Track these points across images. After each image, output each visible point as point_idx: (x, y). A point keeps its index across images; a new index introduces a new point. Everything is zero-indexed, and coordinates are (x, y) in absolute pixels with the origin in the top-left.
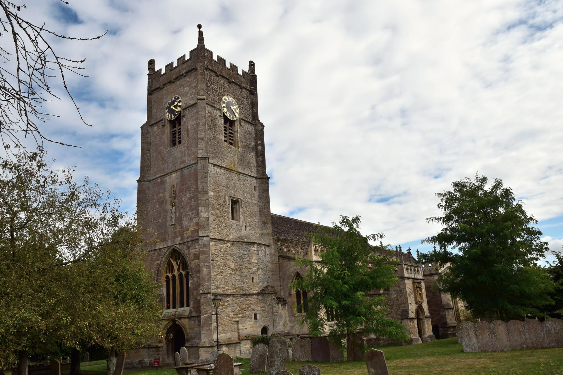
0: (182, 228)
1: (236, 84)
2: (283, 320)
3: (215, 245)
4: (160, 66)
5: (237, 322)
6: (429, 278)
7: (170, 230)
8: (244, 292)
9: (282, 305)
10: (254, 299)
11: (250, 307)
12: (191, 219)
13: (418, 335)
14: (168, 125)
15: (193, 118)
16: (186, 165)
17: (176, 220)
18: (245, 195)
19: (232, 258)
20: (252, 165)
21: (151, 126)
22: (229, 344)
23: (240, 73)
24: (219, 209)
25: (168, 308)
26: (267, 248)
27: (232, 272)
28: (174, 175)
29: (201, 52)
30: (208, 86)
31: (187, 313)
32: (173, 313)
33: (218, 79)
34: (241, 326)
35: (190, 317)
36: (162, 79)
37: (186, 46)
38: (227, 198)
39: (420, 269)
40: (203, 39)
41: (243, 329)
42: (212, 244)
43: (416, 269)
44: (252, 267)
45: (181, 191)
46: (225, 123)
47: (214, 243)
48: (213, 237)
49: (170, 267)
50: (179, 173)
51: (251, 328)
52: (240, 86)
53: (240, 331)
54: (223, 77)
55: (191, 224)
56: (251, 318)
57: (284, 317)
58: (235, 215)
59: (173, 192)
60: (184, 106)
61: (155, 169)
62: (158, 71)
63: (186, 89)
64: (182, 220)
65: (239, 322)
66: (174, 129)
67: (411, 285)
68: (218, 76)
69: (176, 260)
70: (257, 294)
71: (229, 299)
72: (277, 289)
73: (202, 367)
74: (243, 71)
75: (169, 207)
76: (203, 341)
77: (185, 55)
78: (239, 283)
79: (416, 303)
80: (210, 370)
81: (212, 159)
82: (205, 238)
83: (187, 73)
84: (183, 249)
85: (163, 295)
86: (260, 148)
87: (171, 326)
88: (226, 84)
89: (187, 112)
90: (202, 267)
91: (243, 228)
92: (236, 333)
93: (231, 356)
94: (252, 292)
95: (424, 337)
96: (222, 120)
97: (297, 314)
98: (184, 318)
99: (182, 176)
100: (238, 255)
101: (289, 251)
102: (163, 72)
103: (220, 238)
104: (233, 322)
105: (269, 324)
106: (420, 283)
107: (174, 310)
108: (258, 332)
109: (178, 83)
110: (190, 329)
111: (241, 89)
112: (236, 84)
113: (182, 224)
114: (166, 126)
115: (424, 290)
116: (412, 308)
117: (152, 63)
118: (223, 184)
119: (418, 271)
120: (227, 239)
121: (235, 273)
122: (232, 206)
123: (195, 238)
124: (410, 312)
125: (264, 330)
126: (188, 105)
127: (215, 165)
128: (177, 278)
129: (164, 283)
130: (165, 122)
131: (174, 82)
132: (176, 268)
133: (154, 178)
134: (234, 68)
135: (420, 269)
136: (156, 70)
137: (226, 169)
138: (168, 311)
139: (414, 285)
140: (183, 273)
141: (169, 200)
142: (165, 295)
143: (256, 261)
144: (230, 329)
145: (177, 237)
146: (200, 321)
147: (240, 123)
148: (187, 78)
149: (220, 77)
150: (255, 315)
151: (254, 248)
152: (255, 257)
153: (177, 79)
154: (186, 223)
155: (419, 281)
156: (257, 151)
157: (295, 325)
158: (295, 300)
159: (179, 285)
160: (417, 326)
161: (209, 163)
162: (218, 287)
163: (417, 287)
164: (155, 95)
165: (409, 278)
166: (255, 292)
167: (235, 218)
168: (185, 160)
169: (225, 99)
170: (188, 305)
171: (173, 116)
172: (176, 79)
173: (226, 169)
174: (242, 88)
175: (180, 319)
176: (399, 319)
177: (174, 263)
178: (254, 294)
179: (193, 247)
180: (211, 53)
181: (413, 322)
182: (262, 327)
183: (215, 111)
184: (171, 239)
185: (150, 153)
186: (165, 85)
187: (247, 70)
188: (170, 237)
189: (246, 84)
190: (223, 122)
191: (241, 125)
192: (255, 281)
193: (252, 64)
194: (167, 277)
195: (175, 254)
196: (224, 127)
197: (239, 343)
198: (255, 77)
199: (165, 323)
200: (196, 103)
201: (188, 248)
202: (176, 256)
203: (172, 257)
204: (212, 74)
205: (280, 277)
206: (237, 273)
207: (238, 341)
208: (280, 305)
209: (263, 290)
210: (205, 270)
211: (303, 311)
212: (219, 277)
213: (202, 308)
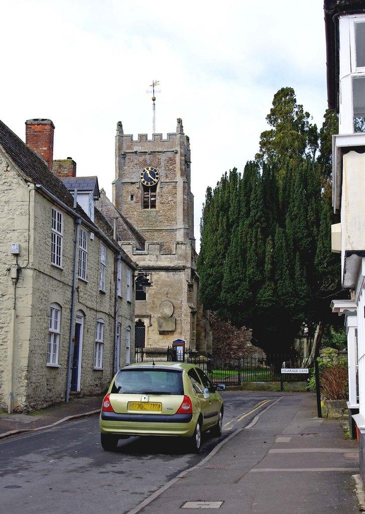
37: (167, 128)
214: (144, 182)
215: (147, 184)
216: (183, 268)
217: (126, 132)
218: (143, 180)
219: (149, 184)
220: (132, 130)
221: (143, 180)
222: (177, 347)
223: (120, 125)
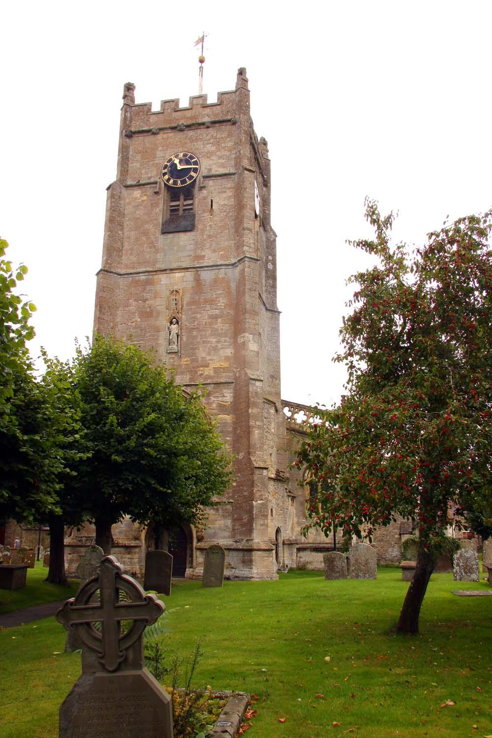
14: (164, 194)
37: (217, 84)
50: (189, 275)
63: (210, 148)
76: (256, 540)
90: (253, 427)
99: (198, 280)
109: (191, 133)
126: (213, 172)
131: (182, 130)
133: (132, 271)
154: (204, 355)
156: (267, 270)
164: (138, 140)
168: (204, 256)
171: (171, 181)
172: (188, 126)
185: (122, 229)
213: (255, 490)
214: (168, 180)
215: (175, 183)
216: (233, 383)
217: (140, 98)
218: (167, 177)
219: (179, 184)
220: (151, 95)
221: (167, 177)
222: (28, 569)
223: (129, 88)
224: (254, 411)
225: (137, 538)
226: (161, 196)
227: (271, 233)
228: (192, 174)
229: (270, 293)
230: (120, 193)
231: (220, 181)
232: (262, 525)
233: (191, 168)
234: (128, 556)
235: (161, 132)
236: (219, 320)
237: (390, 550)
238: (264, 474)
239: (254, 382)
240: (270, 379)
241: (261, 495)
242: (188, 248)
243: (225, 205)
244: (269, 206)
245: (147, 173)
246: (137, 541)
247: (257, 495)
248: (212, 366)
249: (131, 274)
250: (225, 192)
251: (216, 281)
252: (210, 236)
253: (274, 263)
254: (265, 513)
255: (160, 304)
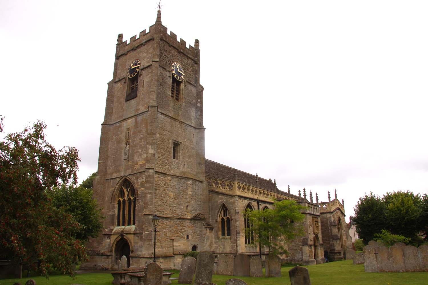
0: (133, 162)
1: (184, 54)
2: (210, 241)
3: (158, 177)
4: (126, 38)
5: (173, 240)
6: (323, 215)
7: (124, 163)
8: (180, 217)
9: (209, 229)
10: (187, 223)
11: (184, 229)
12: (141, 155)
13: (314, 257)
15: (148, 76)
16: (140, 113)
17: (129, 155)
18: (185, 140)
19: (171, 189)
20: (193, 118)
21: (116, 82)
22: (166, 257)
23: (188, 46)
24: (164, 149)
25: (118, 225)
26: (200, 184)
27: (171, 200)
28: (129, 120)
29: (158, 28)
30: (161, 53)
31: (133, 230)
32: (122, 230)
33: (170, 48)
34: (175, 244)
35: (135, 234)
36: (127, 47)
37: (146, 23)
38: (170, 141)
39: (317, 208)
40: (160, 17)
41: (177, 246)
42: (156, 176)
43: (315, 207)
44: (187, 197)
45: (135, 133)
46: (173, 83)
47: (157, 175)
48: (157, 171)
49: (122, 194)
50: (133, 119)
51: (182, 245)
52: (187, 56)
53: (175, 248)
54: (174, 48)
55: (140, 159)
56: (184, 238)
57: (210, 239)
58: (176, 155)
59: (128, 134)
60: (142, 67)
61: (116, 116)
62: (124, 42)
63: (145, 55)
64: (133, 156)
65: (174, 240)
66: (133, 86)
67: (311, 219)
68: (170, 46)
69: (127, 188)
70: (191, 219)
71: (167, 222)
72: (206, 216)
73: (134, 274)
74: (190, 46)
75: (123, 145)
77: (145, 30)
78: (176, 209)
79: (314, 234)
80: (141, 277)
81: (160, 109)
82: (150, 171)
83: (146, 42)
84: (132, 179)
85: (114, 215)
86: (199, 105)
87: (120, 240)
88: (176, 53)
89: (144, 72)
91: (182, 166)
92: (172, 249)
93: (162, 267)
94: (185, 217)
95: (317, 259)
96: (171, 80)
97: (221, 237)
98: (130, 234)
99: (136, 121)
100: (177, 187)
101: (218, 187)
102: (128, 42)
103: (163, 172)
104: (169, 240)
105: (199, 244)
106: (318, 218)
107: (123, 227)
108: (190, 250)
109: (138, 50)
110: (134, 242)
111: (188, 58)
112: (184, 54)
113: (133, 159)
114: (126, 84)
115: (320, 224)
116: (311, 236)
117: (120, 36)
118: (168, 129)
119: (316, 209)
120: (168, 173)
121: (173, 201)
122: (174, 148)
123: (142, 170)
124: (309, 240)
125: (194, 248)
126: (145, 66)
127: (162, 114)
128: (126, 202)
129: (117, 206)
130: (126, 80)
131: (135, 50)
132: (126, 193)
134: (183, 43)
135: (317, 208)
136: (124, 41)
137: (171, 118)
138: (118, 227)
139: (313, 220)
140: (132, 198)
141: (124, 141)
142: (117, 215)
143: (191, 193)
144: (166, 245)
145: (129, 169)
146: (142, 237)
147: (185, 84)
148: (146, 47)
149: (172, 48)
150: (188, 237)
151: (190, 182)
152: (190, 190)
153: (138, 47)
155: (317, 217)
157: (219, 246)
158: (220, 226)
159: (128, 208)
160: (313, 251)
161: (158, 111)
162: (159, 211)
163: (315, 221)
165: (310, 214)
166: (189, 217)
167: (176, 157)
169: (175, 64)
170: (134, 224)
173: (171, 118)
174: (188, 58)
175: (127, 234)
176: (300, 245)
177: (125, 190)
178: (187, 219)
179: (140, 178)
180: (165, 29)
181: (311, 248)
182: (192, 246)
183: (165, 72)
184: (124, 170)
186: (128, 52)
187: (193, 45)
188: (123, 169)
189: (191, 56)
190: (171, 81)
191: (185, 86)
192: (188, 208)
193: (197, 42)
194: (119, 201)
195: (126, 183)
196: (172, 85)
197: (174, 257)
198: (199, 51)
199: (116, 236)
200: (151, 65)
201: (137, 178)
202: (127, 185)
203: (123, 185)
204: (166, 44)
205: (209, 207)
206: (175, 201)
207: (173, 255)
208: (208, 229)
209: (195, 216)
210: (149, 196)
211: (226, 235)
212: (160, 203)
215: (131, 76)
224: (147, 185)
225: (111, 251)
226: (127, 84)
227: (200, 87)
228: (137, 70)
229: (199, 119)
230: (112, 86)
231: (147, 70)
232: (147, 245)
233: (136, 67)
234: (107, 260)
235: (129, 53)
236: (143, 140)
237: (297, 255)
238: (150, 218)
239: (148, 170)
240: (198, 165)
241: (148, 229)
242: (134, 106)
243: (148, 81)
244: (199, 73)
245: (123, 74)
246: (111, 253)
247: (145, 229)
248: (139, 164)
249: (114, 124)
250: (148, 75)
251: (142, 120)
252: (142, 99)
253: (202, 103)
254: (150, 238)
255: (123, 136)
